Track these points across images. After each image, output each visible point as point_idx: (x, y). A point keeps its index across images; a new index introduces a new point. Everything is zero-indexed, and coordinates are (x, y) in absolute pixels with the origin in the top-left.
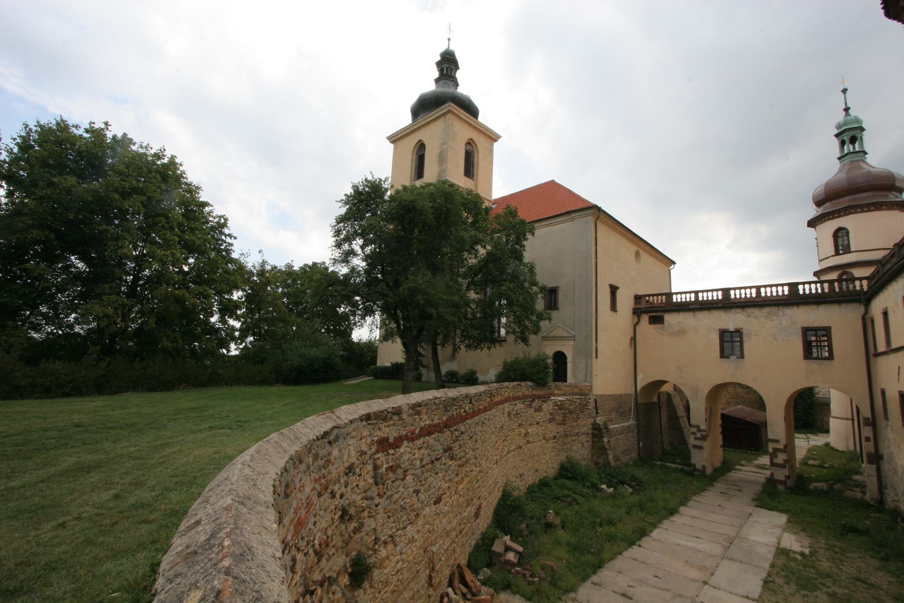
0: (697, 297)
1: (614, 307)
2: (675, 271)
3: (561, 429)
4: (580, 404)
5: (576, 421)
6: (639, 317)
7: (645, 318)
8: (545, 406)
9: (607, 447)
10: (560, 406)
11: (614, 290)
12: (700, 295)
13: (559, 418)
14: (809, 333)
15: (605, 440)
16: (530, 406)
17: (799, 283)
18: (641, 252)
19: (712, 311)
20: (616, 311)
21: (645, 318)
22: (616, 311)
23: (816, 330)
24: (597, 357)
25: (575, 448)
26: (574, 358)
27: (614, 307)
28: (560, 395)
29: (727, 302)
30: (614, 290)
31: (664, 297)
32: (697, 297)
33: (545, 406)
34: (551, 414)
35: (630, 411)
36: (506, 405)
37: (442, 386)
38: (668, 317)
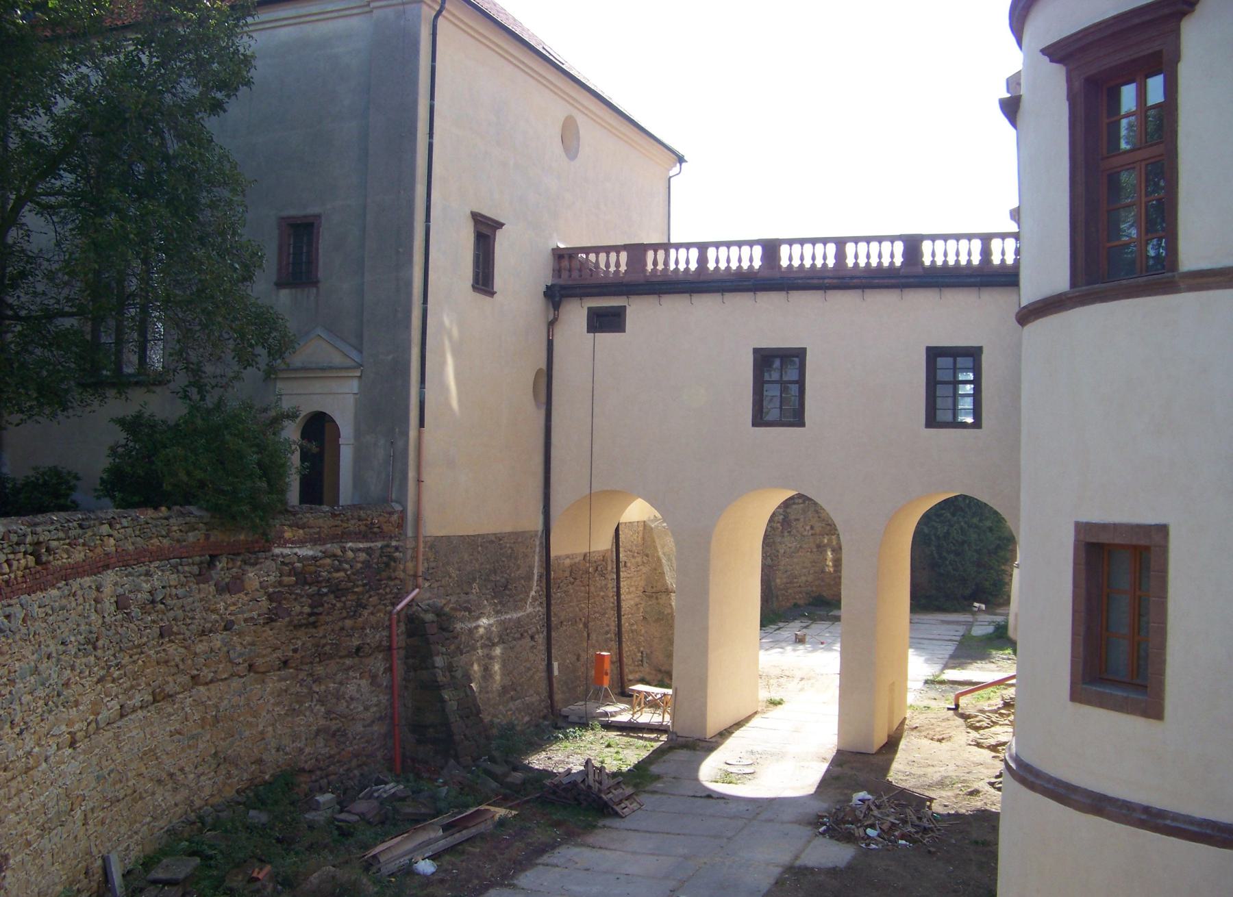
0: (840, 255)
1: (483, 280)
2: (683, 183)
3: (303, 639)
4: (367, 564)
5: (355, 615)
6: (556, 306)
7: (576, 314)
8: (253, 578)
9: (441, 678)
10: (303, 575)
11: (485, 232)
12: (850, 248)
13: (300, 608)
14: (942, 362)
15: (439, 661)
16: (201, 577)
17: (922, 238)
18: (581, 119)
19: (906, 291)
20: (492, 293)
21: (576, 314)
22: (492, 293)
23: (954, 353)
24: (422, 423)
25: (351, 689)
26: (358, 434)
27: (483, 280)
28: (302, 543)
29: (771, 279)
30: (485, 232)
31: (624, 256)
32: (840, 255)
33: (253, 578)
34: (270, 598)
35: (529, 578)
36: (109, 578)
37: (413, 600)
38: (638, 311)
